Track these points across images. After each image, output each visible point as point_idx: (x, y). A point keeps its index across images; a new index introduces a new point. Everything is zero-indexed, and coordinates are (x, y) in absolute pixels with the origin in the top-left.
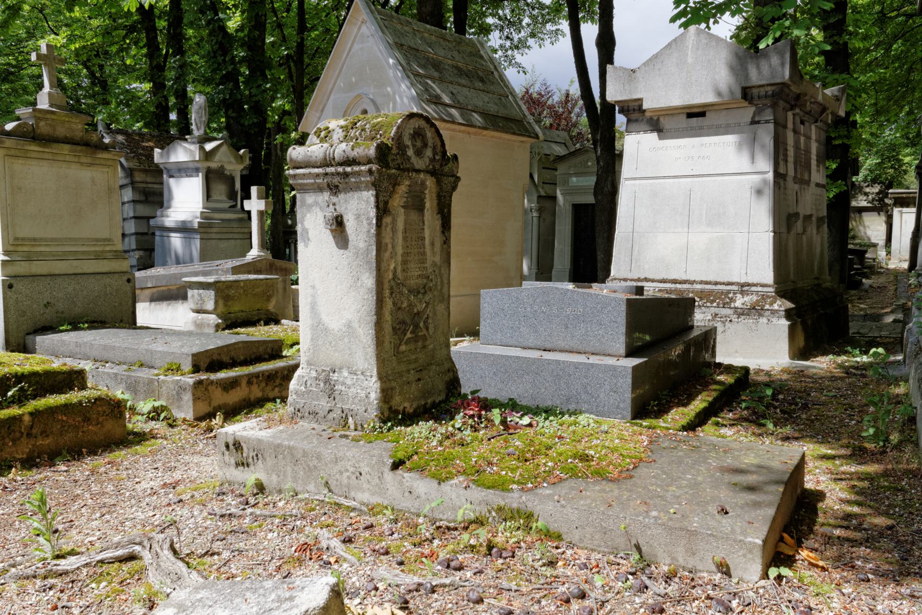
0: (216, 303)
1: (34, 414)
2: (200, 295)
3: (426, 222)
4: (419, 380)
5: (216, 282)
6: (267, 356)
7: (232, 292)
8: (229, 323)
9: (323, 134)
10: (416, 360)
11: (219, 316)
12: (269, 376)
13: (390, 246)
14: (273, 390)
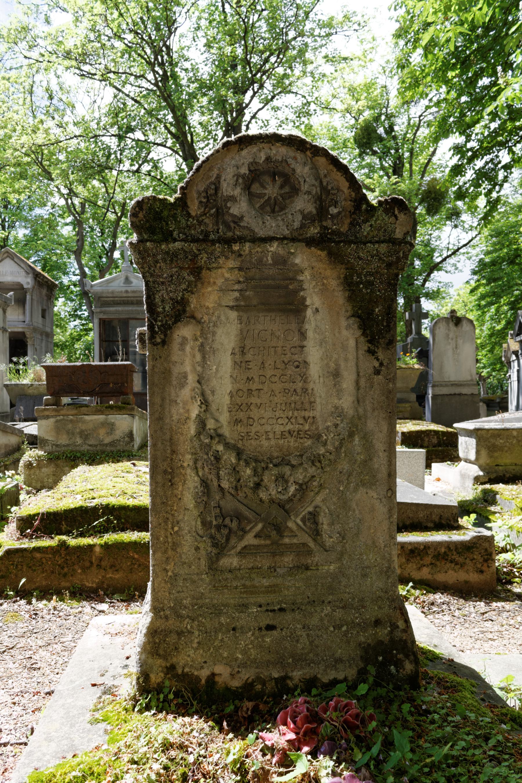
0: (478, 452)
1: (106, 546)
2: (466, 442)
3: (310, 334)
4: (270, 628)
5: (477, 430)
6: (431, 525)
7: (500, 442)
8: (493, 476)
9: (272, 190)
10: (272, 589)
11: (481, 468)
12: (412, 551)
13: (192, 379)
14: (419, 569)
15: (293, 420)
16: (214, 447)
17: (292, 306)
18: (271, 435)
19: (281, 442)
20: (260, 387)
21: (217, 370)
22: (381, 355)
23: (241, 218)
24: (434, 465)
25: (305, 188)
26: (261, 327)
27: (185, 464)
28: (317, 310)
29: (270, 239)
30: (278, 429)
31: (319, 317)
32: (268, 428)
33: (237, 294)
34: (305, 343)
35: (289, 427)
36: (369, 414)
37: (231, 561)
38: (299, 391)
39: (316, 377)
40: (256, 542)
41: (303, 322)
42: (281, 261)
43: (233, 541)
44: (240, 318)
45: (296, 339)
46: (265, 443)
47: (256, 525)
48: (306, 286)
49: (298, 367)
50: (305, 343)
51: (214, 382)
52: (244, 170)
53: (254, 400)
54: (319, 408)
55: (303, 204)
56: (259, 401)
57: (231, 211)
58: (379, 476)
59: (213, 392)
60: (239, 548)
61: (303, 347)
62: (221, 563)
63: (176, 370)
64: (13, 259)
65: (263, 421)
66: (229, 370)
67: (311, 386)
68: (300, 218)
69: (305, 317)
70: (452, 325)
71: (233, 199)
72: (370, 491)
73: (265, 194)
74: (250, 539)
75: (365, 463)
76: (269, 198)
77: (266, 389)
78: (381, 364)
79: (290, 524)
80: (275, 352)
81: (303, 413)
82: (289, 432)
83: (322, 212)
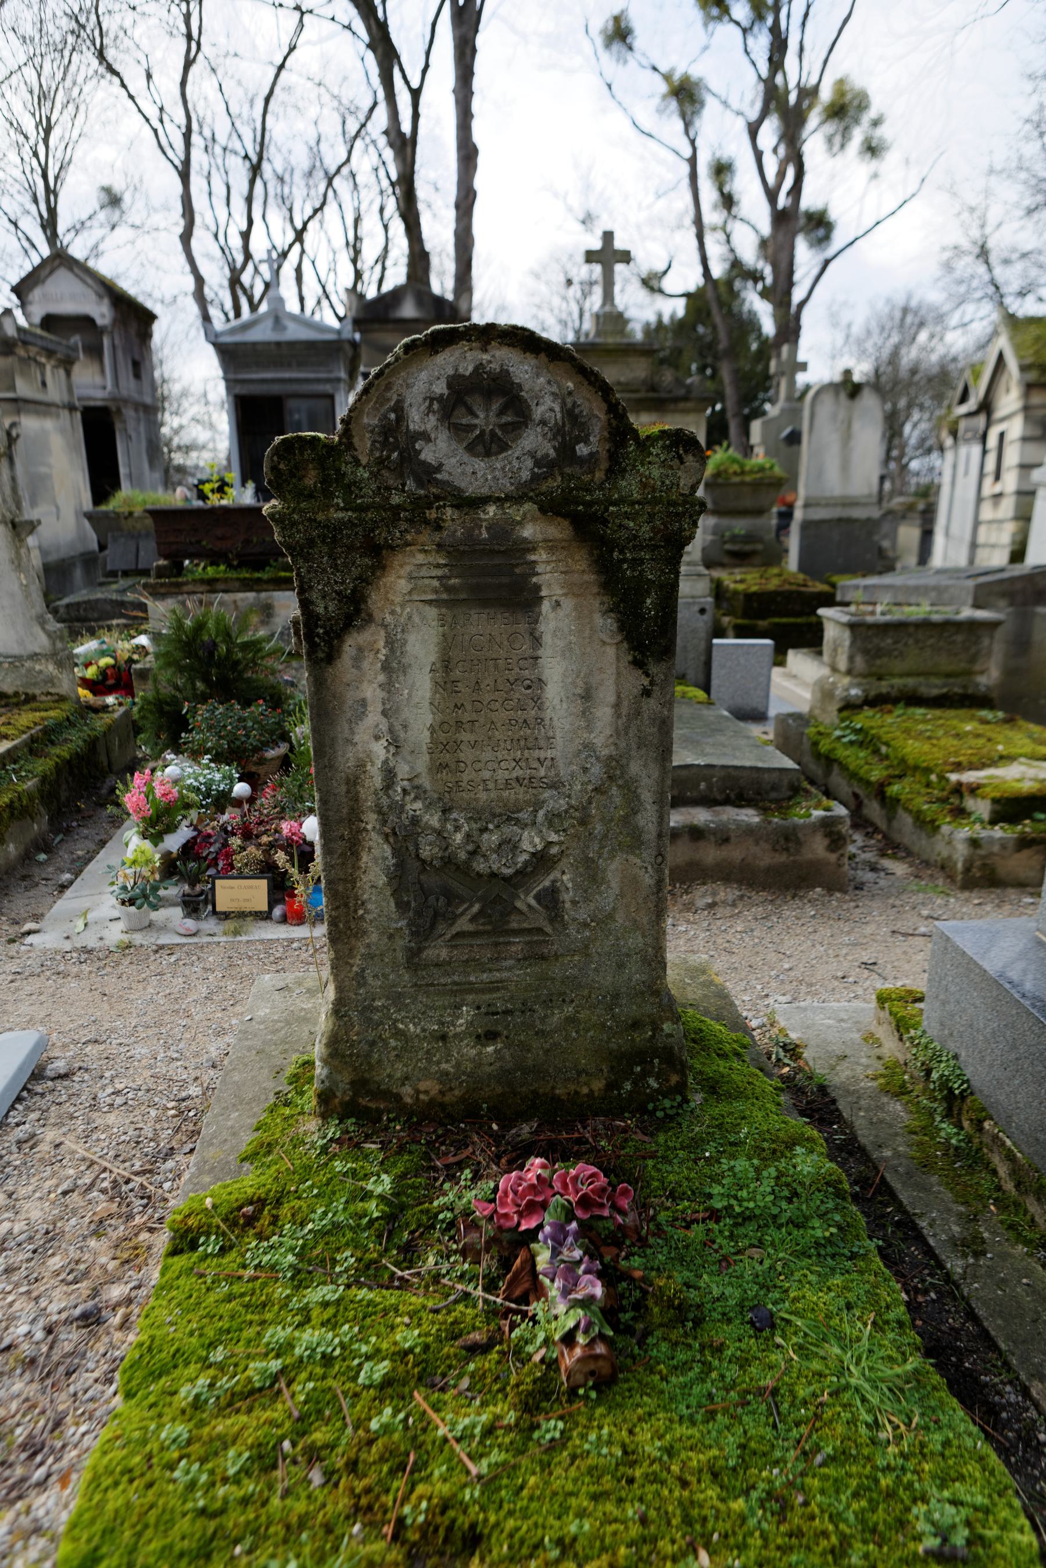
3: (547, 639)
9: (485, 418)
15: (523, 764)
16: (408, 807)
17: (520, 598)
18: (491, 785)
19: (506, 794)
20: (474, 717)
21: (410, 695)
22: (653, 669)
23: (439, 468)
24: (791, 653)
25: (538, 412)
26: (473, 630)
27: (369, 827)
28: (558, 604)
29: (485, 500)
30: (502, 775)
31: (561, 613)
32: (486, 774)
33: (436, 583)
34: (540, 653)
35: (518, 772)
36: (633, 753)
37: (437, 951)
38: (531, 722)
39: (556, 701)
40: (471, 928)
41: (537, 621)
42: (502, 531)
43: (441, 927)
44: (442, 619)
45: (526, 648)
46: (483, 796)
47: (471, 906)
48: (540, 569)
49: (529, 687)
50: (540, 653)
51: (406, 714)
52: (440, 388)
53: (465, 736)
54: (559, 741)
55: (534, 441)
56: (472, 738)
57: (422, 457)
58: (646, 837)
59: (405, 727)
60: (448, 936)
61: (537, 658)
62: (424, 955)
63: (351, 696)
64: (71, 269)
65: (478, 766)
66: (428, 695)
67: (548, 714)
68: (529, 463)
69: (540, 613)
70: (843, 396)
71: (425, 436)
72: (631, 858)
73: (475, 426)
74: (463, 924)
75: (626, 820)
76: (483, 432)
77: (482, 720)
78: (652, 683)
79: (519, 904)
80: (496, 667)
81: (536, 753)
82: (517, 779)
83: (566, 452)
